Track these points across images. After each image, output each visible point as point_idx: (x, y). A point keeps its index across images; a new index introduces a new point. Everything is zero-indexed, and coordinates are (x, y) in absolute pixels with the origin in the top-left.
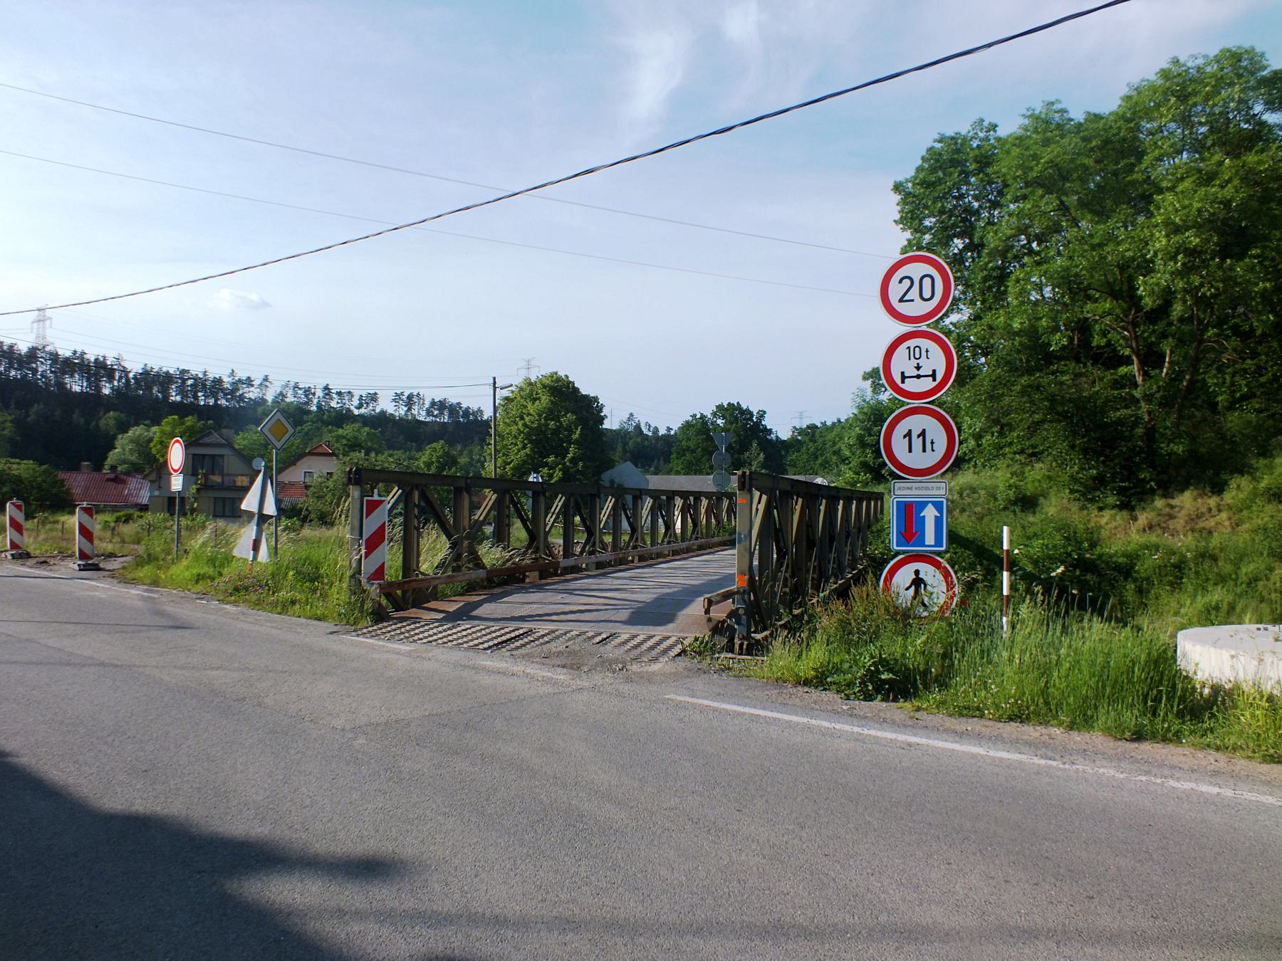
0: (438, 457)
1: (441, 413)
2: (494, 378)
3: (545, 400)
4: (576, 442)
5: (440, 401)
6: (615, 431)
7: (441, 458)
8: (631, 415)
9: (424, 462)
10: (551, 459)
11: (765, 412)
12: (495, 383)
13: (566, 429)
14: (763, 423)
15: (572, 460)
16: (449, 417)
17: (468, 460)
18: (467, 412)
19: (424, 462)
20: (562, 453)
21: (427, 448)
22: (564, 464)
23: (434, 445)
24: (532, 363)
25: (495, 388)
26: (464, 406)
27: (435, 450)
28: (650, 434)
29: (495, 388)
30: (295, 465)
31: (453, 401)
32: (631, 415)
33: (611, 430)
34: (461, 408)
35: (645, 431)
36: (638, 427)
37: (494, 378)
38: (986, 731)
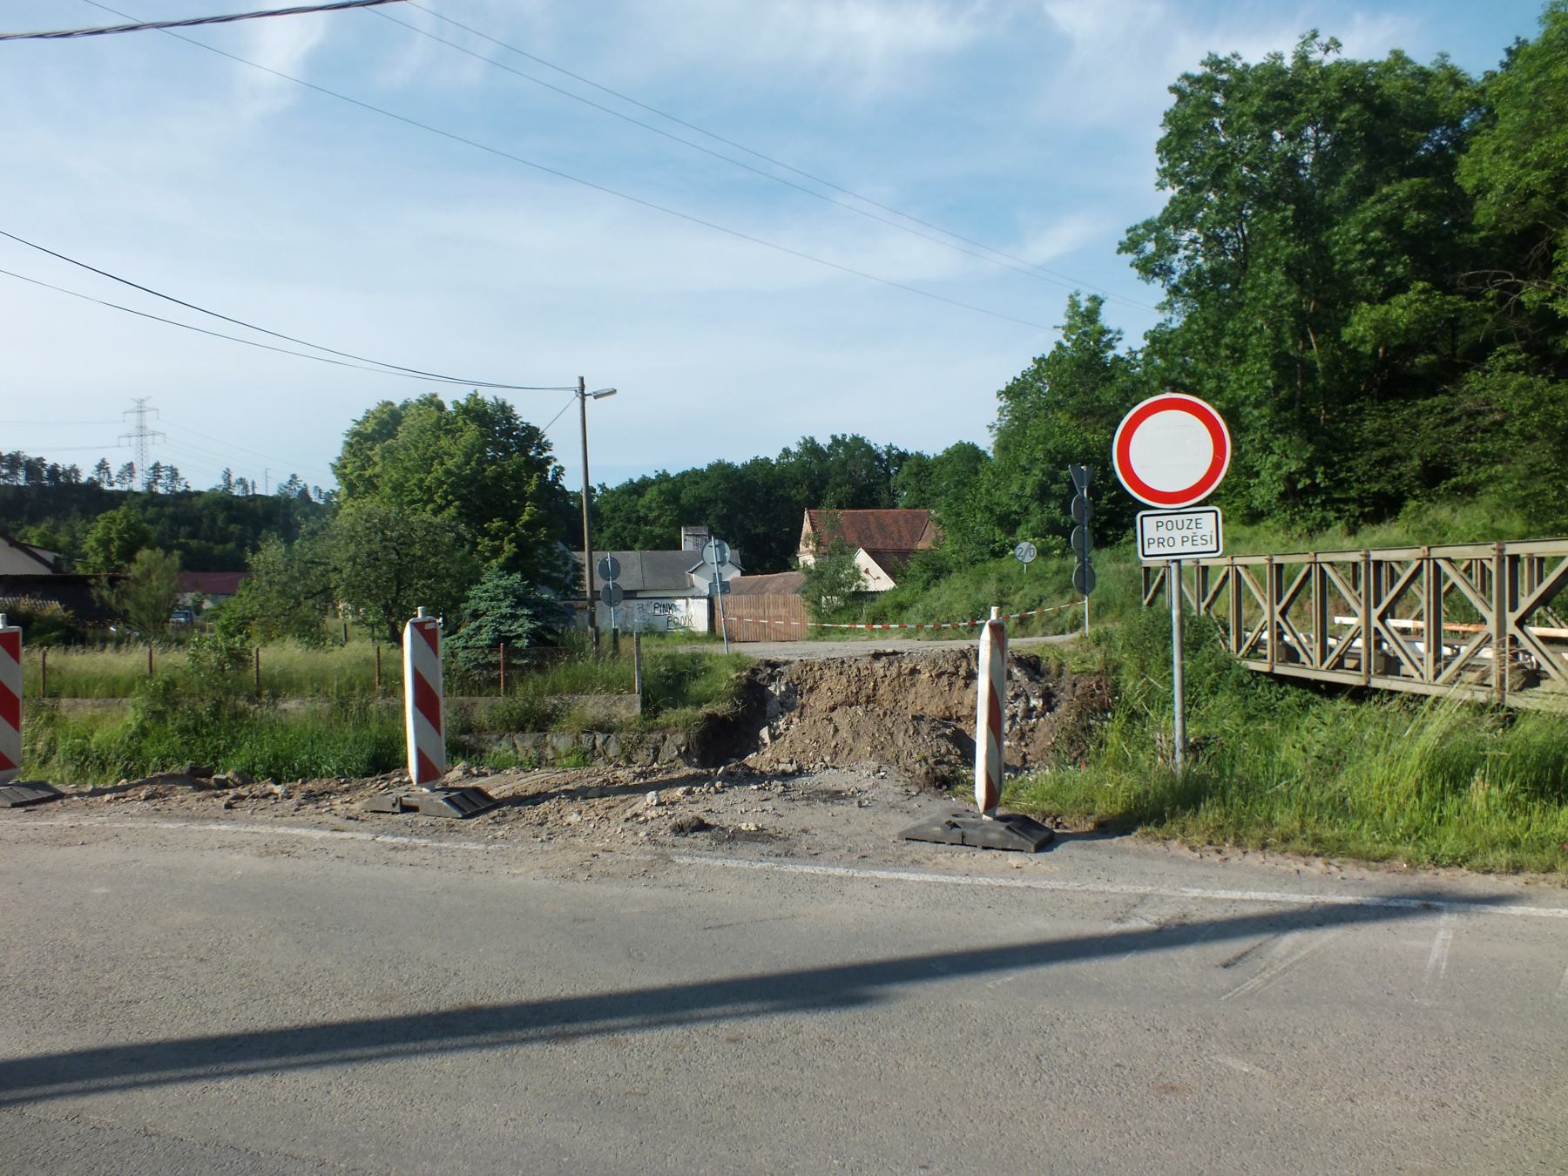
0: (119, 532)
1: (14, 473)
2: (582, 379)
3: (471, 433)
4: (533, 497)
5: (10, 455)
6: (272, 498)
7: (126, 532)
8: (294, 476)
9: (98, 540)
10: (497, 523)
11: (562, 469)
12: (583, 387)
13: (512, 478)
14: (561, 482)
15: (527, 526)
16: (27, 479)
17: (68, 539)
18: (54, 471)
19: (98, 540)
20: (512, 516)
21: (99, 517)
22: (516, 530)
23: (110, 513)
24: (147, 404)
25: (583, 396)
26: (49, 462)
27: (113, 520)
28: (321, 502)
29: (583, 396)
30: (11, 545)
31: (31, 454)
32: (294, 476)
33: (267, 498)
34: (44, 465)
35: (314, 497)
36: (304, 493)
37: (582, 379)
38: (1276, 906)
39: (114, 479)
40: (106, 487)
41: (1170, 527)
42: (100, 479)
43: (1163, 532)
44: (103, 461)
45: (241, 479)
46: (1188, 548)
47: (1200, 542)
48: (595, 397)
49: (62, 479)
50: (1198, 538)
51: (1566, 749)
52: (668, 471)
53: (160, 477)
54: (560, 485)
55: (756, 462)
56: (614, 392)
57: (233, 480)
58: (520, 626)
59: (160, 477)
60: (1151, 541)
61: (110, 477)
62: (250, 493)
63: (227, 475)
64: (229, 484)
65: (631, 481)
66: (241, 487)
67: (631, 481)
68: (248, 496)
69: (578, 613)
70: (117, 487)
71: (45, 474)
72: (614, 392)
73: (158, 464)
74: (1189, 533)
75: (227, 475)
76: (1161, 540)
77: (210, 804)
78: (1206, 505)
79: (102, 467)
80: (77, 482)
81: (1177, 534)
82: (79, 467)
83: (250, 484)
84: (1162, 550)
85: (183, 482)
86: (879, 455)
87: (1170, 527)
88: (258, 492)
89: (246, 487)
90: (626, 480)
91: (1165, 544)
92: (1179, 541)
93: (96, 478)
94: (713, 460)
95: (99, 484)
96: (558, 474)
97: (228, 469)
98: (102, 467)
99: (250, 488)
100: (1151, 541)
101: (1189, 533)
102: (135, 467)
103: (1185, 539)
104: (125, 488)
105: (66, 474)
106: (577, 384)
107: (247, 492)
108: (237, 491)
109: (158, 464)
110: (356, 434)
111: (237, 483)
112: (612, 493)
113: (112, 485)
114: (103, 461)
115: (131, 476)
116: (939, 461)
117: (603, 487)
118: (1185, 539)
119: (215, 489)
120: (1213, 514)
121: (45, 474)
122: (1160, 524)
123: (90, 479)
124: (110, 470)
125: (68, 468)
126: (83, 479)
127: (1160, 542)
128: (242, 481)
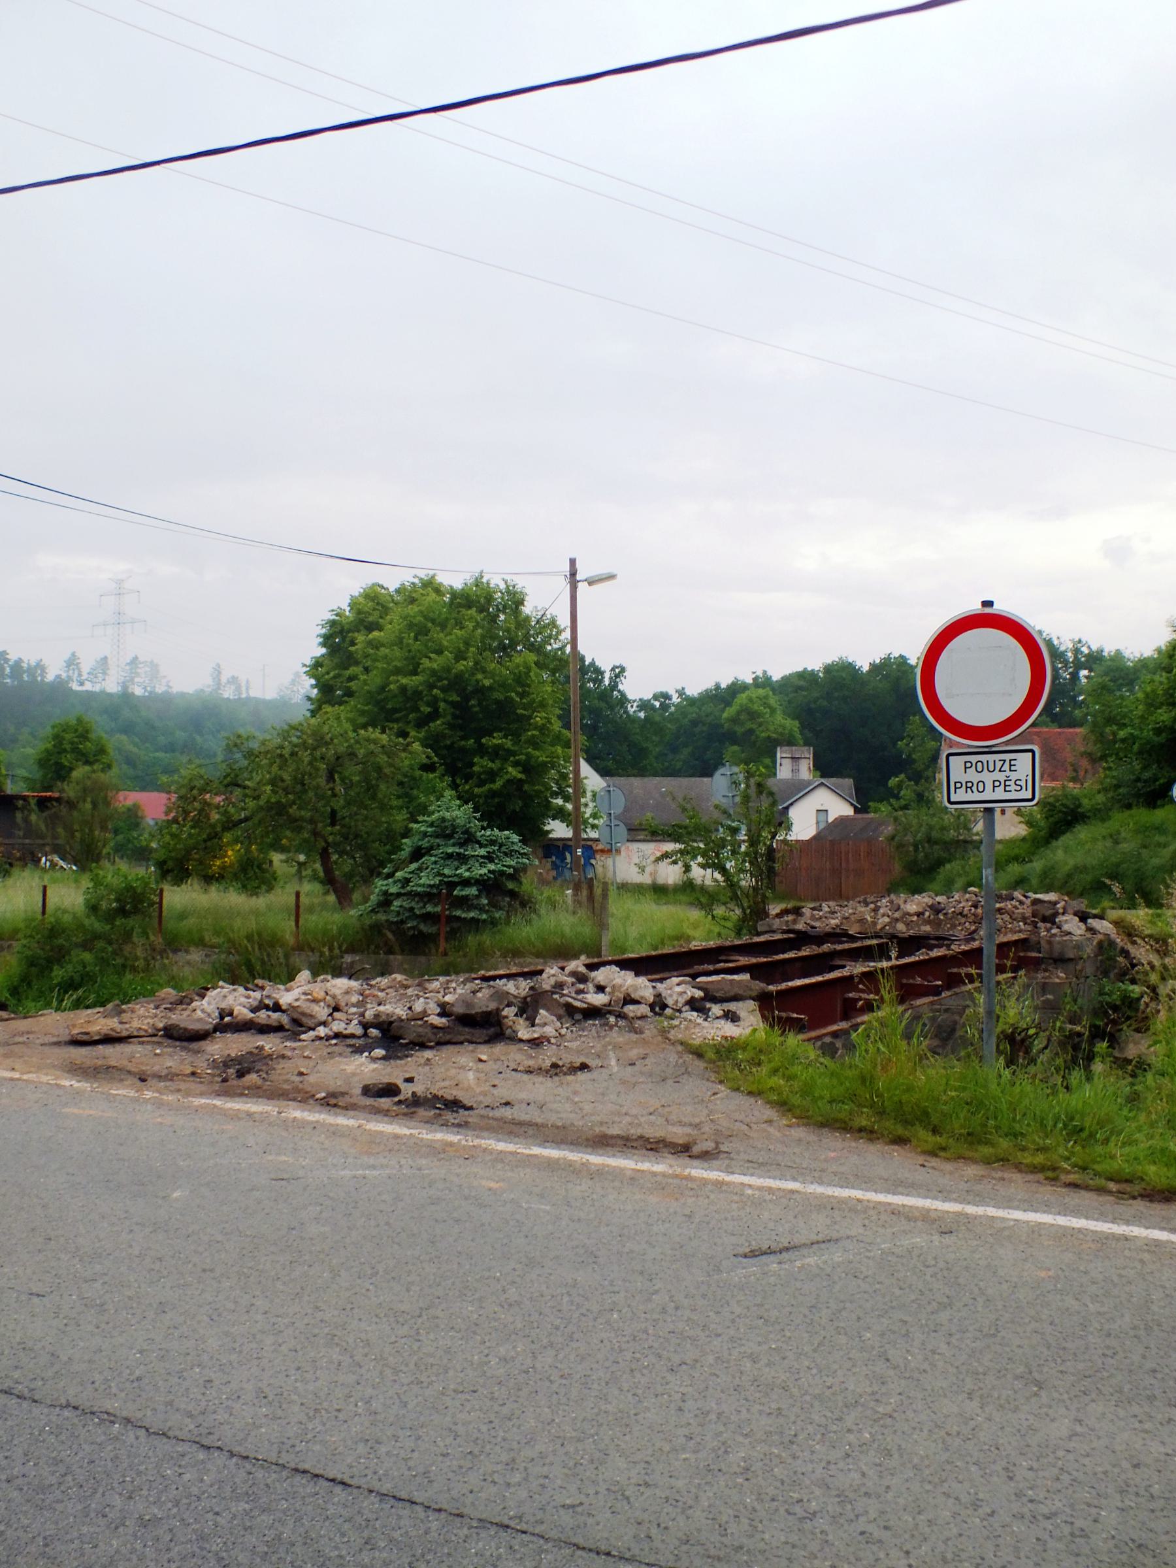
2: (573, 562)
6: (270, 701)
12: (573, 574)
26: (13, 657)
34: (7, 661)
37: (573, 562)
39: (85, 676)
40: (75, 687)
41: (980, 768)
42: (68, 676)
43: (972, 776)
44: (73, 654)
45: (233, 677)
46: (1000, 794)
47: (1013, 787)
48: (590, 584)
49: (25, 677)
50: (1012, 783)
51: (1, 1006)
52: (769, 673)
53: (138, 675)
54: (619, 691)
55: (886, 663)
56: (611, 577)
57: (224, 679)
58: (468, 870)
59: (138, 675)
60: (958, 785)
61: (80, 675)
62: (244, 696)
63: (218, 671)
64: (219, 684)
65: (718, 686)
66: (233, 687)
67: (718, 686)
68: (240, 699)
69: (598, 857)
70: (88, 687)
71: (8, 670)
72: (611, 577)
73: (136, 658)
74: (1001, 777)
75: (218, 671)
76: (969, 785)
77: (588, 1108)
78: (1016, 744)
79: (72, 662)
80: (42, 680)
81: (988, 778)
82: (45, 662)
83: (243, 684)
84: (970, 797)
85: (164, 681)
86: (1063, 654)
87: (980, 768)
88: (253, 694)
89: (238, 688)
90: (710, 685)
91: (974, 788)
92: (989, 786)
93: (64, 675)
94: (830, 658)
95: (67, 682)
96: (617, 676)
97: (218, 665)
98: (72, 662)
99: (244, 689)
100: (958, 785)
101: (1001, 777)
102: (109, 661)
103: (997, 784)
104: (97, 688)
105: (31, 671)
106: (566, 568)
107: (240, 693)
108: (228, 693)
109: (136, 658)
110: (333, 623)
111: (229, 682)
112: (692, 701)
113: (82, 684)
114: (73, 654)
115: (104, 673)
116: (1143, 663)
117: (681, 693)
118: (997, 784)
119: (202, 690)
120: (1030, 754)
121: (8, 670)
122: (968, 765)
123: (58, 676)
124: (81, 666)
125: (33, 664)
126: (50, 677)
127: (969, 786)
128: (234, 680)
